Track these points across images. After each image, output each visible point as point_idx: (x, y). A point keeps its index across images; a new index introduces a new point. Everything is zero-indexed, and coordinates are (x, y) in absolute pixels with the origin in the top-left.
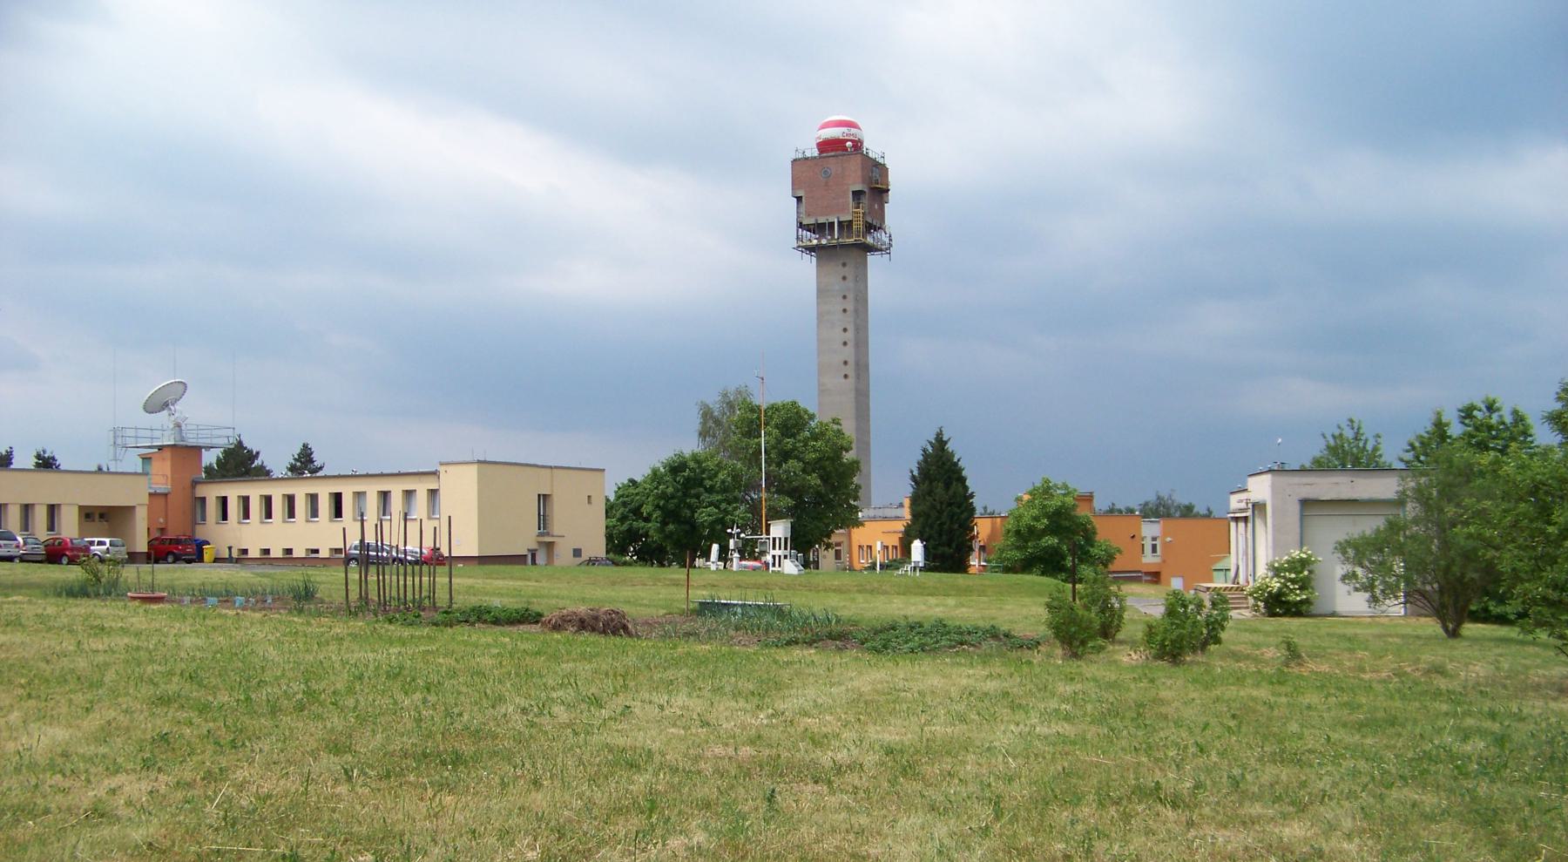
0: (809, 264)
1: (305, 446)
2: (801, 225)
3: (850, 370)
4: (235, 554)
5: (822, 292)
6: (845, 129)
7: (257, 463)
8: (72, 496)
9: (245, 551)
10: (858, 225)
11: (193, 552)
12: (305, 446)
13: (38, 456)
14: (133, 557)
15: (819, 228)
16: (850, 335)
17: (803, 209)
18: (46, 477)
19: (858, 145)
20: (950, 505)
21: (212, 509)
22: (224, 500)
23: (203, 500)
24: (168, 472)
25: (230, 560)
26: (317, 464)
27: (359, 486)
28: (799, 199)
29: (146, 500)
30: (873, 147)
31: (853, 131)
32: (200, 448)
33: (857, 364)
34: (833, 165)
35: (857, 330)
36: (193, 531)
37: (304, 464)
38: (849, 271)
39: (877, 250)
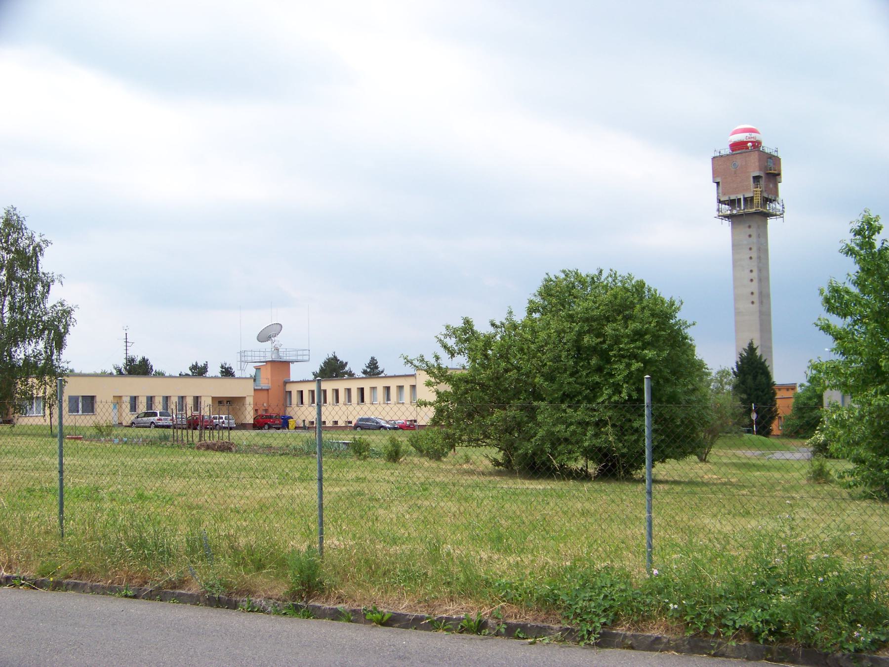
0: (727, 225)
1: (373, 359)
2: (720, 202)
3: (755, 298)
4: (307, 424)
5: (735, 246)
6: (747, 134)
7: (347, 369)
8: (209, 389)
9: (336, 422)
10: (757, 200)
11: (284, 423)
12: (373, 359)
13: (222, 367)
14: (242, 426)
15: (732, 203)
16: (755, 275)
17: (720, 191)
18: (228, 381)
19: (757, 144)
20: (756, 390)
21: (295, 398)
22: (337, 391)
23: (290, 392)
24: (269, 377)
25: (304, 428)
26: (380, 369)
27: (400, 382)
28: (718, 183)
29: (252, 393)
30: (768, 146)
31: (753, 135)
32: (287, 363)
33: (761, 293)
34: (739, 160)
35: (760, 270)
36: (285, 411)
37: (373, 370)
38: (753, 231)
39: (776, 215)
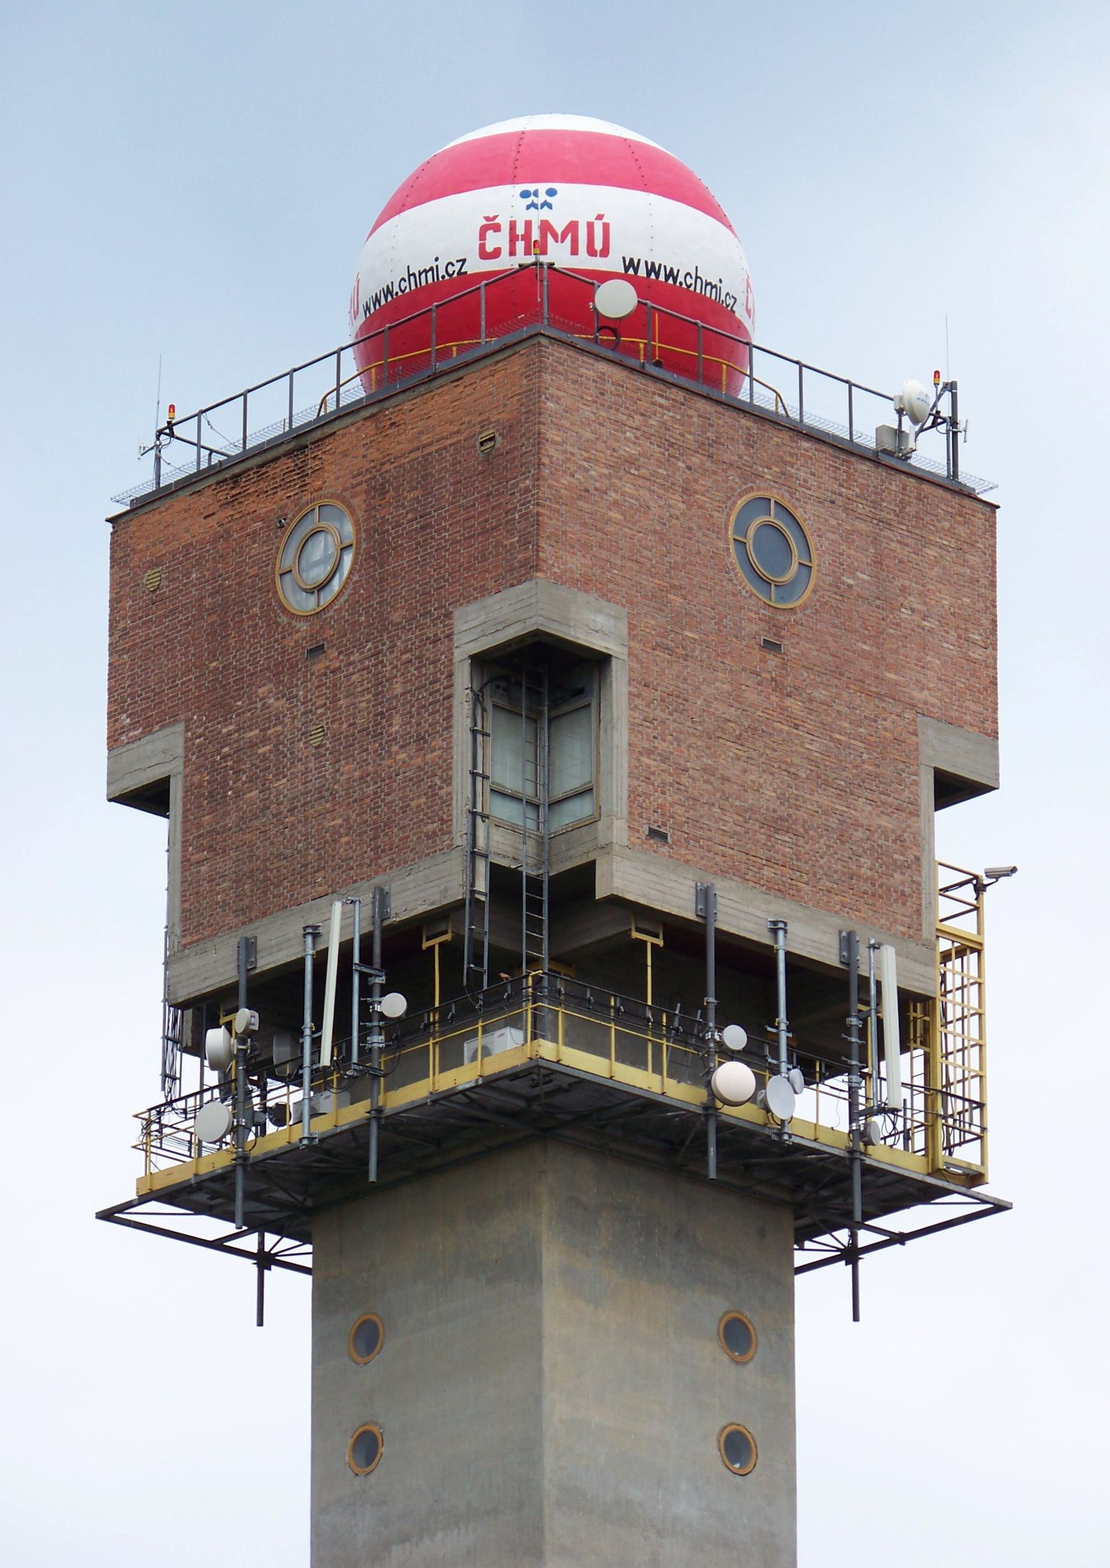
6: (504, 201)
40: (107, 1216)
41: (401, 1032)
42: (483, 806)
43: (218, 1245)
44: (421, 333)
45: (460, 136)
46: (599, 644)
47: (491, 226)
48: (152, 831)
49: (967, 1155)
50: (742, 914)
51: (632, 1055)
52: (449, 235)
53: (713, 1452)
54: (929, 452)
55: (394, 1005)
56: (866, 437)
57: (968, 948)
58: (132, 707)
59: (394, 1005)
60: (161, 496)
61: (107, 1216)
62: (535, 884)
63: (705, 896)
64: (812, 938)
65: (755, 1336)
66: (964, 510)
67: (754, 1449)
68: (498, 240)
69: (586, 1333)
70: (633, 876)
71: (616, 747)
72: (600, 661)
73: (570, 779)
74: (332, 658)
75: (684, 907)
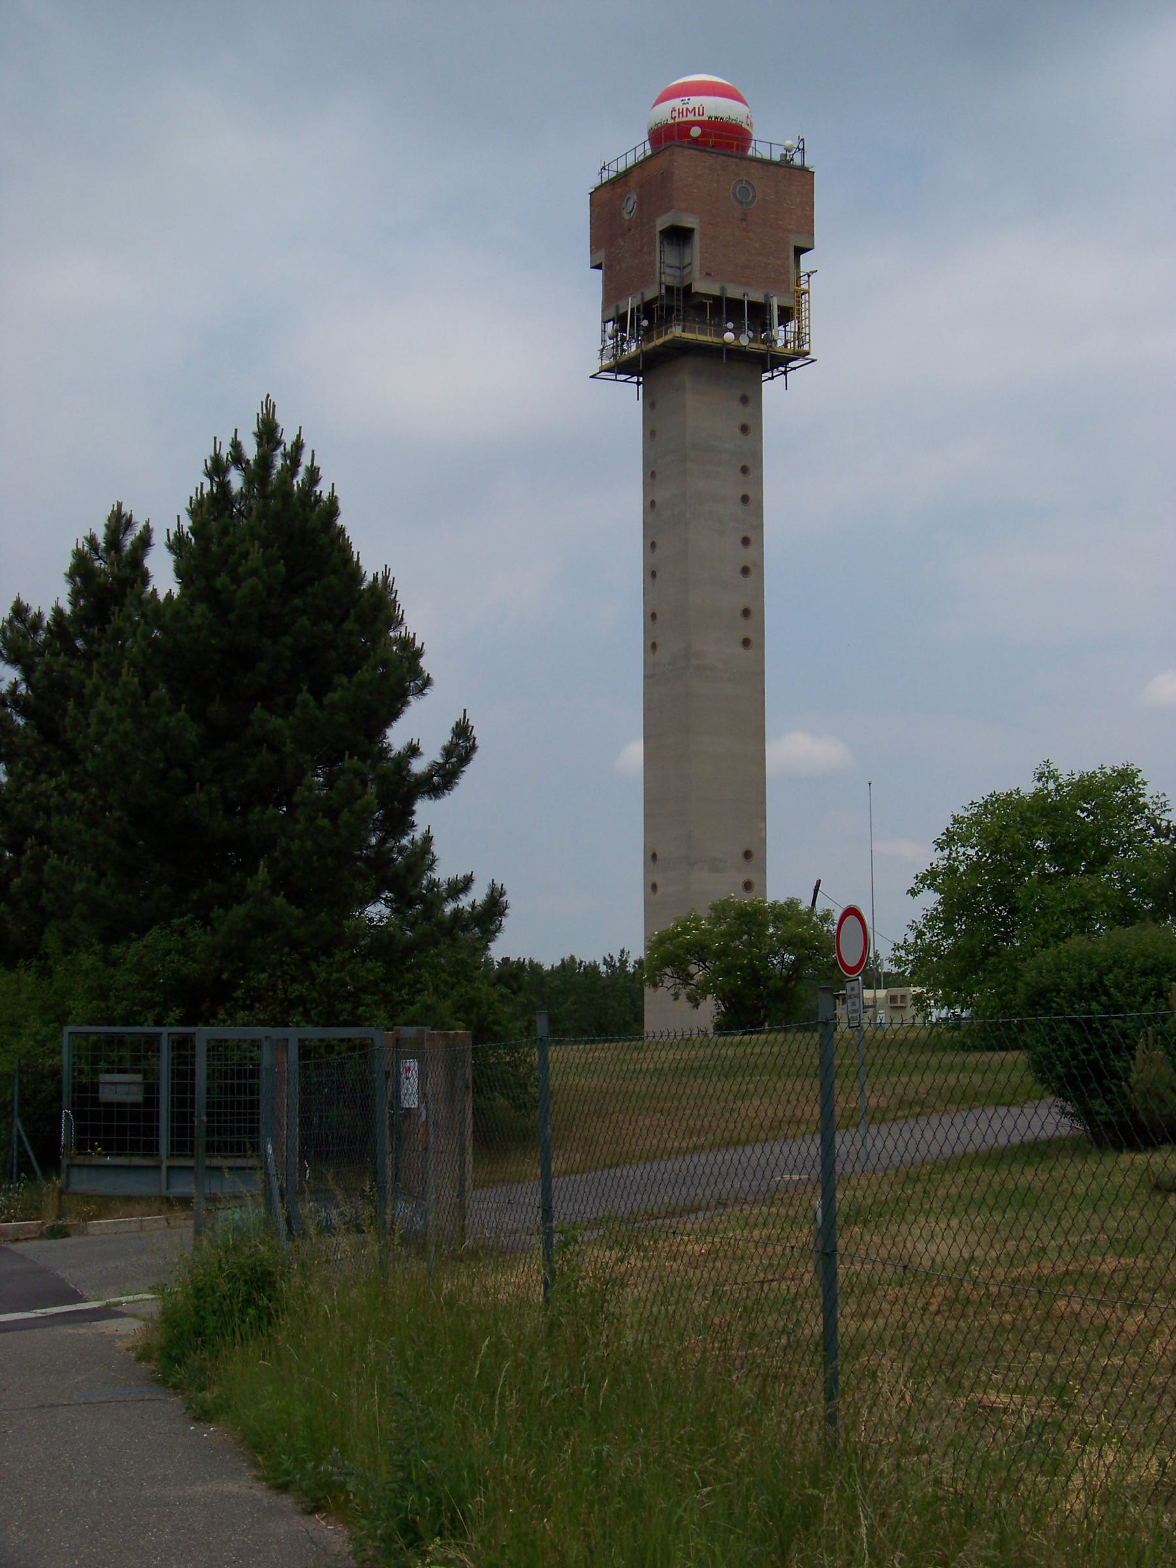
6: (676, 103)
40: (592, 377)
41: (648, 330)
42: (664, 271)
43: (625, 381)
44: (666, 137)
45: (685, 76)
46: (690, 226)
47: (673, 110)
48: (599, 273)
49: (806, 348)
50: (734, 292)
51: (703, 332)
52: (664, 113)
53: (737, 431)
54: (797, 161)
55: (645, 323)
56: (776, 157)
57: (807, 292)
58: (595, 245)
59: (645, 323)
60: (602, 185)
61: (592, 377)
62: (678, 290)
63: (723, 289)
64: (756, 296)
65: (751, 400)
66: (805, 174)
67: (750, 429)
68: (676, 114)
69: (701, 406)
70: (699, 287)
71: (696, 251)
72: (691, 230)
73: (687, 261)
74: (633, 231)
75: (717, 293)
